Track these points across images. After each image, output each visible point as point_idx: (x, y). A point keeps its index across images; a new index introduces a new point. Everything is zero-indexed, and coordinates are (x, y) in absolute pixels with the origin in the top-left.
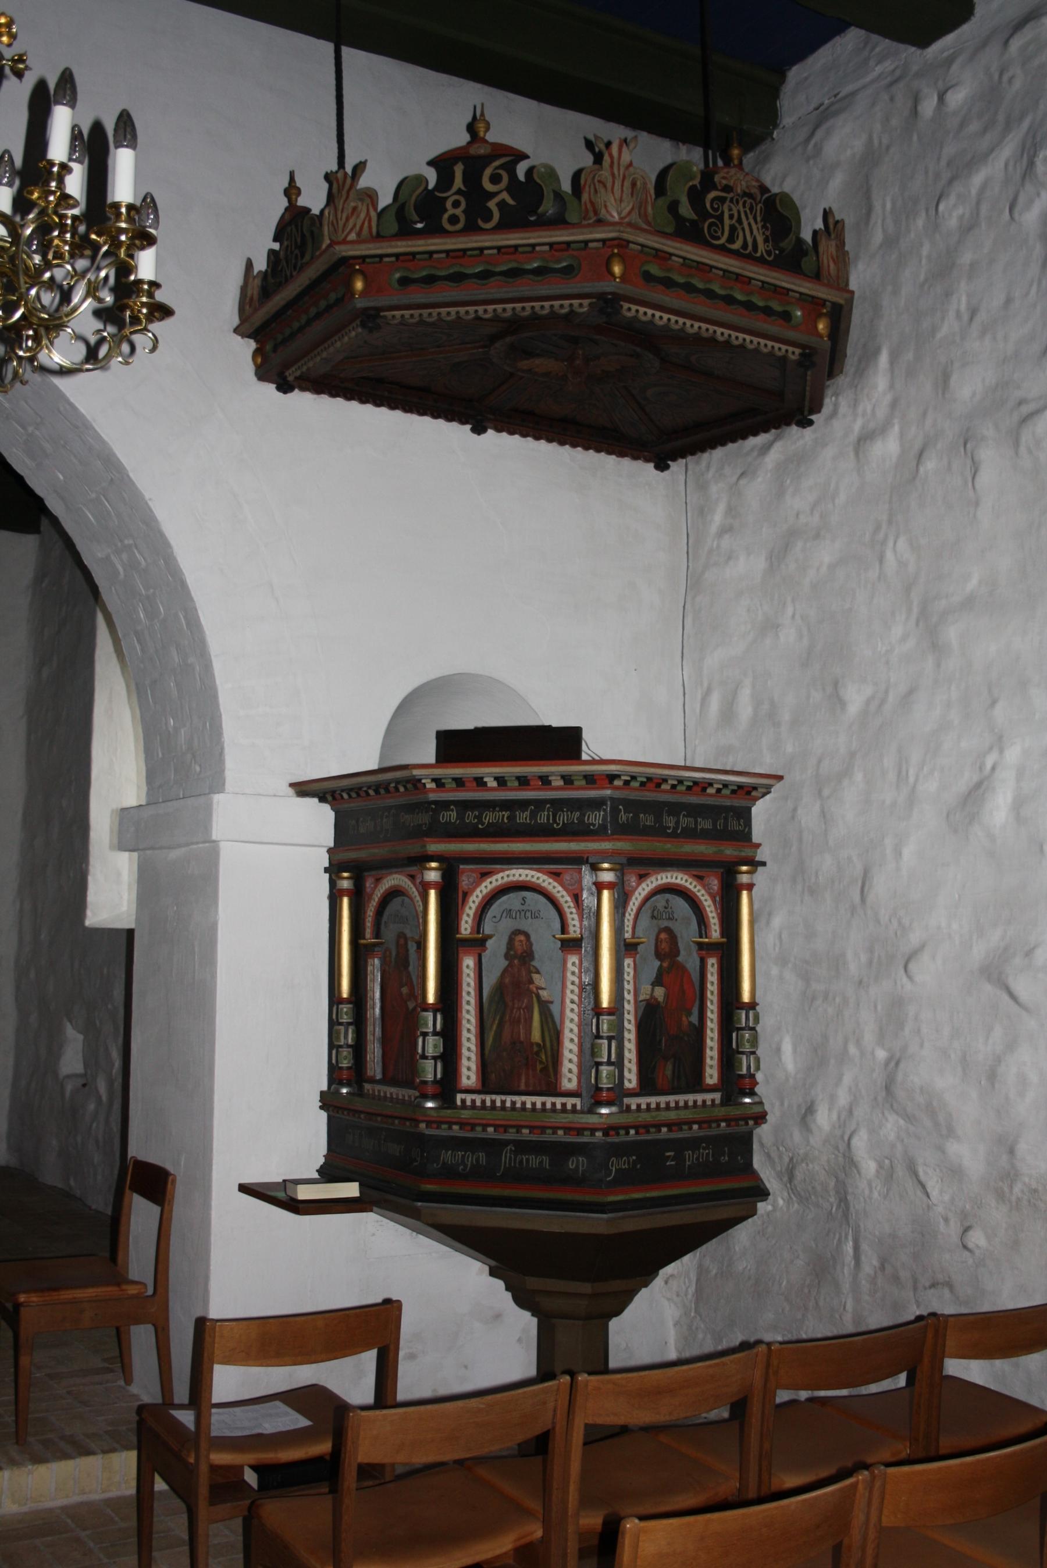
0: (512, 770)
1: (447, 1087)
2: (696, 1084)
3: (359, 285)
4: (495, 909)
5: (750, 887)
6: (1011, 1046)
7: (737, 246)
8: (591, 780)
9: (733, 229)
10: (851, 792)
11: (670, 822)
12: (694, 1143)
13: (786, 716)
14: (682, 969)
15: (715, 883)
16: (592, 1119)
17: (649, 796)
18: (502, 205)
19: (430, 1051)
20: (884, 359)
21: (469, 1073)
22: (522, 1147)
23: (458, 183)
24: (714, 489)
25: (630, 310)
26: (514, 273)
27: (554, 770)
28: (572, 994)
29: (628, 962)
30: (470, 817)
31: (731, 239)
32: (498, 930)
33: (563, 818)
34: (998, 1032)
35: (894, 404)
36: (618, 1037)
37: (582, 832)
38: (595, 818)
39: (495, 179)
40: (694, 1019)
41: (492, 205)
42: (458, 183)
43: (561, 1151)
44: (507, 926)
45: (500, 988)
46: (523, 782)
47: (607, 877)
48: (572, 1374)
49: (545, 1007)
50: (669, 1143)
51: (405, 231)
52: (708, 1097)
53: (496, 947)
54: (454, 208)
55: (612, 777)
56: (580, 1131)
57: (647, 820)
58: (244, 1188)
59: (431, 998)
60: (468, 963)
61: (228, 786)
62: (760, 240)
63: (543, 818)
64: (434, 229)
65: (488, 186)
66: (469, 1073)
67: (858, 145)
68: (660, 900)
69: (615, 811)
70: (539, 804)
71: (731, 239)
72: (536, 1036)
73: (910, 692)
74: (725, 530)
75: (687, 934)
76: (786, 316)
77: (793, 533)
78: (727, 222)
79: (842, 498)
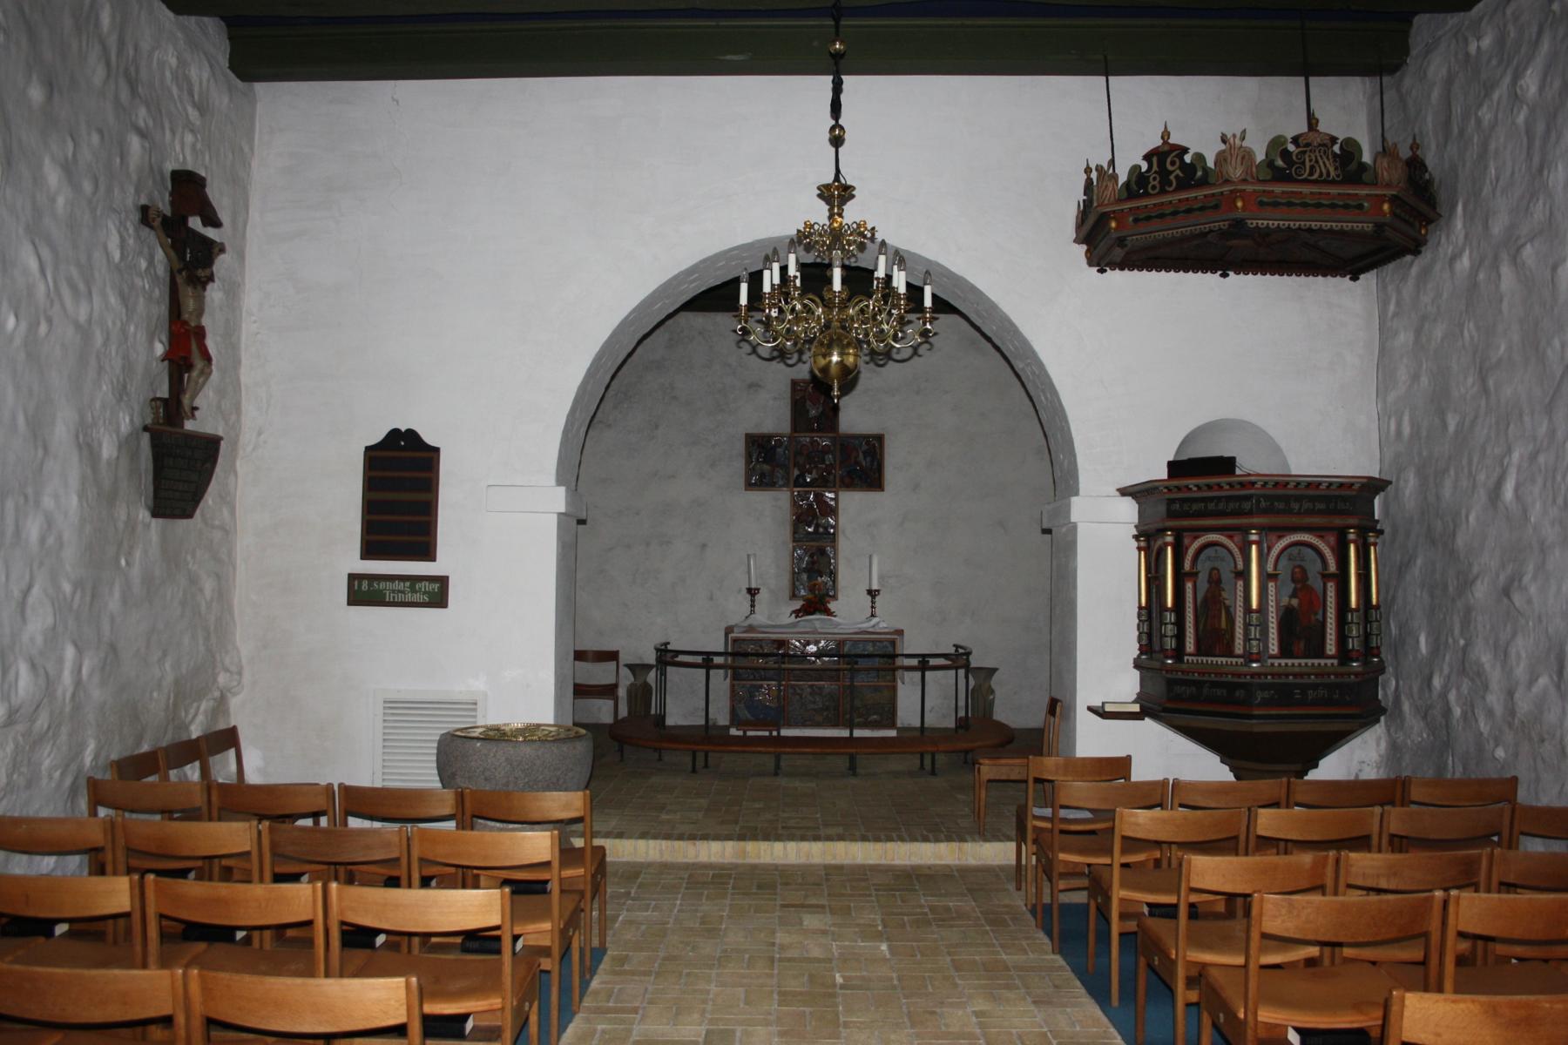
0: (1202, 481)
1: (1179, 653)
2: (1321, 653)
3: (1113, 225)
4: (1203, 556)
5: (1375, 544)
6: (1514, 635)
7: (1315, 176)
8: (1242, 485)
9: (1312, 167)
10: (1448, 483)
11: (1296, 506)
12: (1315, 686)
13: (1424, 434)
14: (1310, 590)
15: (1332, 540)
16: (1245, 669)
17: (1280, 492)
18: (1177, 177)
19: (1169, 633)
20: (1460, 208)
21: (1190, 646)
22: (1214, 684)
23: (1155, 167)
24: (1390, 288)
25: (1252, 224)
26: (1189, 211)
27: (1223, 480)
28: (1240, 602)
29: (1271, 585)
30: (1186, 507)
31: (1311, 174)
32: (1204, 567)
33: (1232, 506)
34: (1509, 629)
35: (1466, 237)
36: (1247, 626)
37: (1239, 513)
38: (1247, 506)
39: (1173, 163)
40: (1320, 617)
41: (1172, 177)
42: (1155, 167)
43: (1232, 687)
44: (1208, 565)
45: (1205, 599)
46: (1209, 487)
47: (1254, 538)
48: (1446, 890)
49: (1227, 609)
50: (1296, 686)
51: (1137, 196)
52: (1329, 662)
53: (1203, 579)
54: (1154, 182)
55: (1253, 484)
56: (1239, 675)
57: (1280, 505)
58: (1090, 709)
59: (1169, 604)
60: (1189, 586)
61: (1081, 492)
62: (1332, 169)
63: (1221, 506)
64: (1147, 195)
65: (1170, 168)
66: (1190, 646)
67: (1444, 71)
68: (1295, 550)
69: (1258, 502)
70: (1219, 499)
71: (1311, 174)
72: (1223, 625)
73: (1476, 417)
74: (1396, 315)
75: (1314, 568)
76: (1360, 207)
77: (1424, 318)
78: (1308, 164)
79: (1445, 295)
